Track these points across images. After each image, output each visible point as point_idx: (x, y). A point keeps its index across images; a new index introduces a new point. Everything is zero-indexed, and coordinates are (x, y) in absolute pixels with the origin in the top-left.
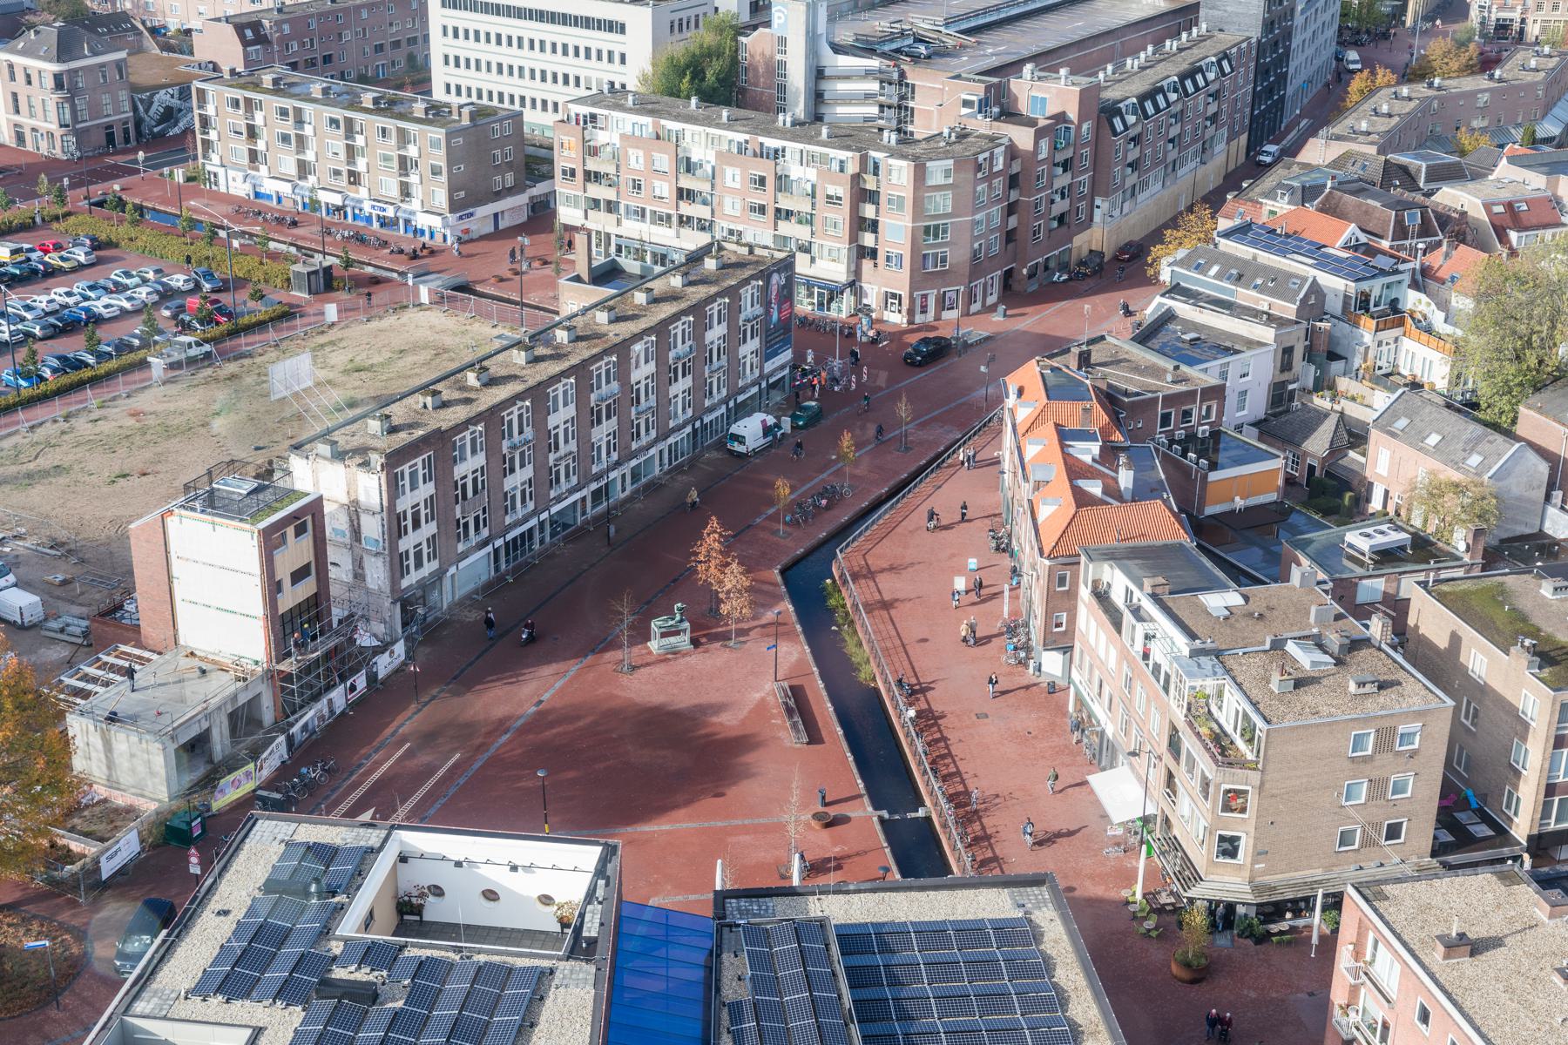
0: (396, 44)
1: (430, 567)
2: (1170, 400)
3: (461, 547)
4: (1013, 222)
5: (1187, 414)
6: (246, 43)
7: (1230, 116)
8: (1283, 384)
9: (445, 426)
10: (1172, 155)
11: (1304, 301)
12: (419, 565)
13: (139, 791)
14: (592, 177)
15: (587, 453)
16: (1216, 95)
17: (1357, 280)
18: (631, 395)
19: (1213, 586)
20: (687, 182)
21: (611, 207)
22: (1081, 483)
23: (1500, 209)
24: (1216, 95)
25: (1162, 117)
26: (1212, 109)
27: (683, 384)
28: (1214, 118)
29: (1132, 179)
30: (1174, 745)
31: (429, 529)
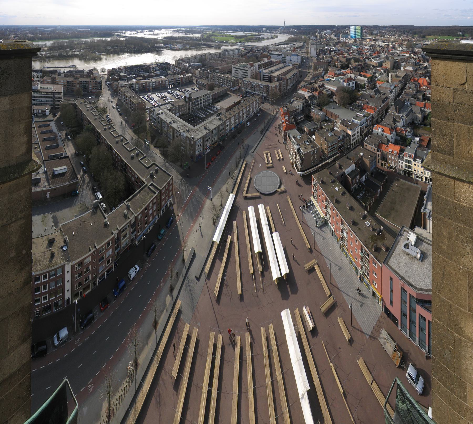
18: (240, 117)
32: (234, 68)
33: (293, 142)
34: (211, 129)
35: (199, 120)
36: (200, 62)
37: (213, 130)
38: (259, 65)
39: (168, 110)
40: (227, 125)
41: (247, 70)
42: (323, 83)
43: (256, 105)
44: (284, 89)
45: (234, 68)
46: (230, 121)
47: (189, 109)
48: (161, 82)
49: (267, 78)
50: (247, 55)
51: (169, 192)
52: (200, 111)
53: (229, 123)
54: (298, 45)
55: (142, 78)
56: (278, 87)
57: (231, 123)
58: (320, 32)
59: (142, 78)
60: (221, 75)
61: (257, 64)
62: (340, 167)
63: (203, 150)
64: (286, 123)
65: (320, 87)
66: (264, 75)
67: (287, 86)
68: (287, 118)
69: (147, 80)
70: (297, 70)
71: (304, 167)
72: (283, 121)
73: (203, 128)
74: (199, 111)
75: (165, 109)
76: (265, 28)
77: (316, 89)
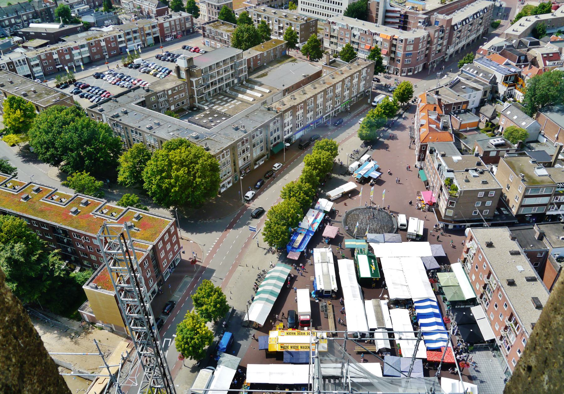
1: (290, 134)
2: (455, 104)
3: (297, 129)
4: (427, 52)
10: (469, 34)
11: (491, 80)
12: (288, 133)
14: (332, 36)
15: (325, 108)
17: (348, 215)
18: (317, 106)
20: (353, 39)
21: (336, 44)
22: (430, 125)
23: (545, 56)
24: (482, 18)
25: (478, 19)
26: (480, 22)
28: (481, 24)
30: (441, 189)
35: (218, 118)
39: (138, 104)
40: (286, 121)
43: (359, 82)
44: (439, 51)
47: (192, 97)
48: (103, 44)
49: (397, 17)
51: (173, 245)
52: (221, 99)
53: (291, 118)
56: (422, 47)
60: (269, 9)
62: (542, 236)
63: (235, 171)
64: (430, 128)
66: (387, 11)
67: (449, 43)
68: (433, 117)
69: (60, 46)
71: (455, 214)
72: (424, 122)
74: (218, 100)
75: (131, 102)
77: (534, 62)
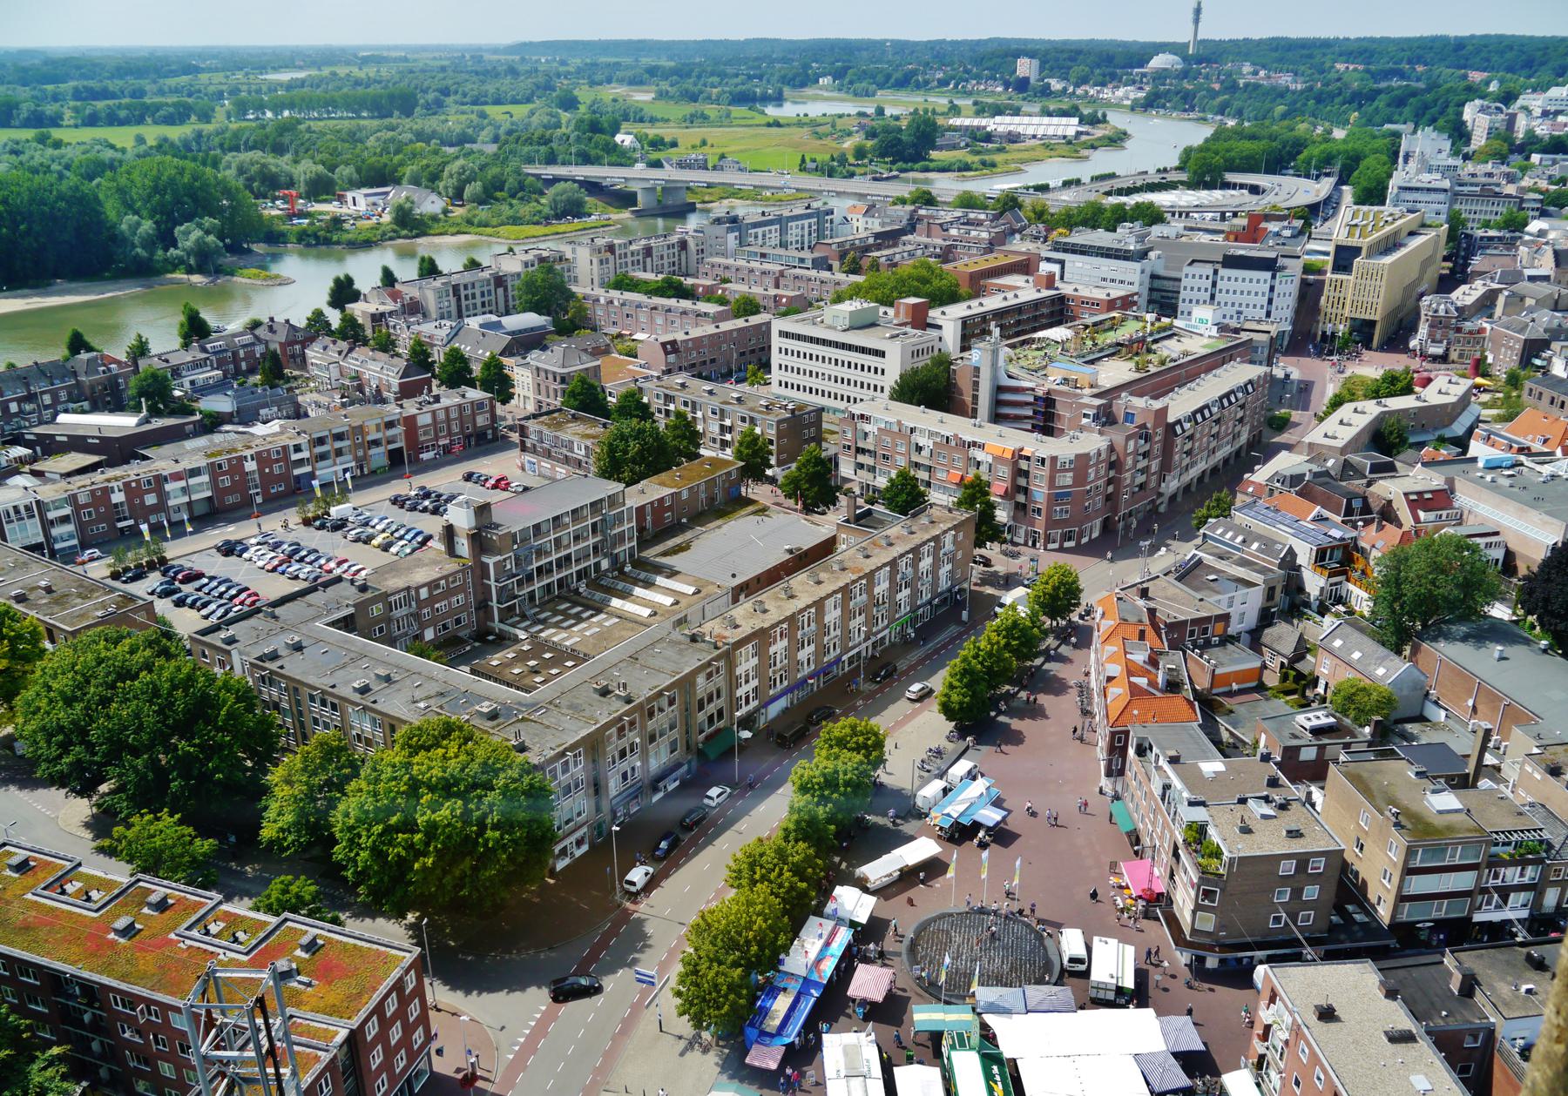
0: (753, 351)
1: (753, 704)
2: (1195, 622)
4: (1110, 489)
5: (1205, 631)
6: (667, 353)
7: (1252, 417)
8: (1268, 609)
9: (766, 625)
12: (747, 702)
13: (819, 129)
16: (1242, 407)
19: (1207, 758)
21: (872, 469)
22: (1133, 679)
24: (1242, 407)
26: (1240, 414)
27: (906, 592)
28: (1241, 420)
29: (1187, 461)
30: (1176, 855)
31: (754, 683)
32: (785, 334)
33: (1166, 787)
34: (642, 692)
36: (537, 308)
37: (649, 700)
38: (965, 323)
39: (333, 624)
40: (740, 671)
41: (881, 354)
42: (1450, 482)
44: (1142, 486)
45: (785, 334)
46: (761, 652)
48: (251, 466)
50: (881, 255)
52: (563, 612)
53: (755, 661)
54: (1291, 195)
55: (95, 459)
57: (765, 661)
58: (1508, 98)
59: (95, 459)
61: (958, 311)
64: (1133, 687)
65: (1419, 501)
66: (1000, 389)
67: (1166, 467)
68: (1140, 657)
70: (1255, 371)
71: (1220, 926)
72: (1115, 669)
73: (588, 695)
74: (556, 613)
75: (314, 619)
76: (1031, 55)
